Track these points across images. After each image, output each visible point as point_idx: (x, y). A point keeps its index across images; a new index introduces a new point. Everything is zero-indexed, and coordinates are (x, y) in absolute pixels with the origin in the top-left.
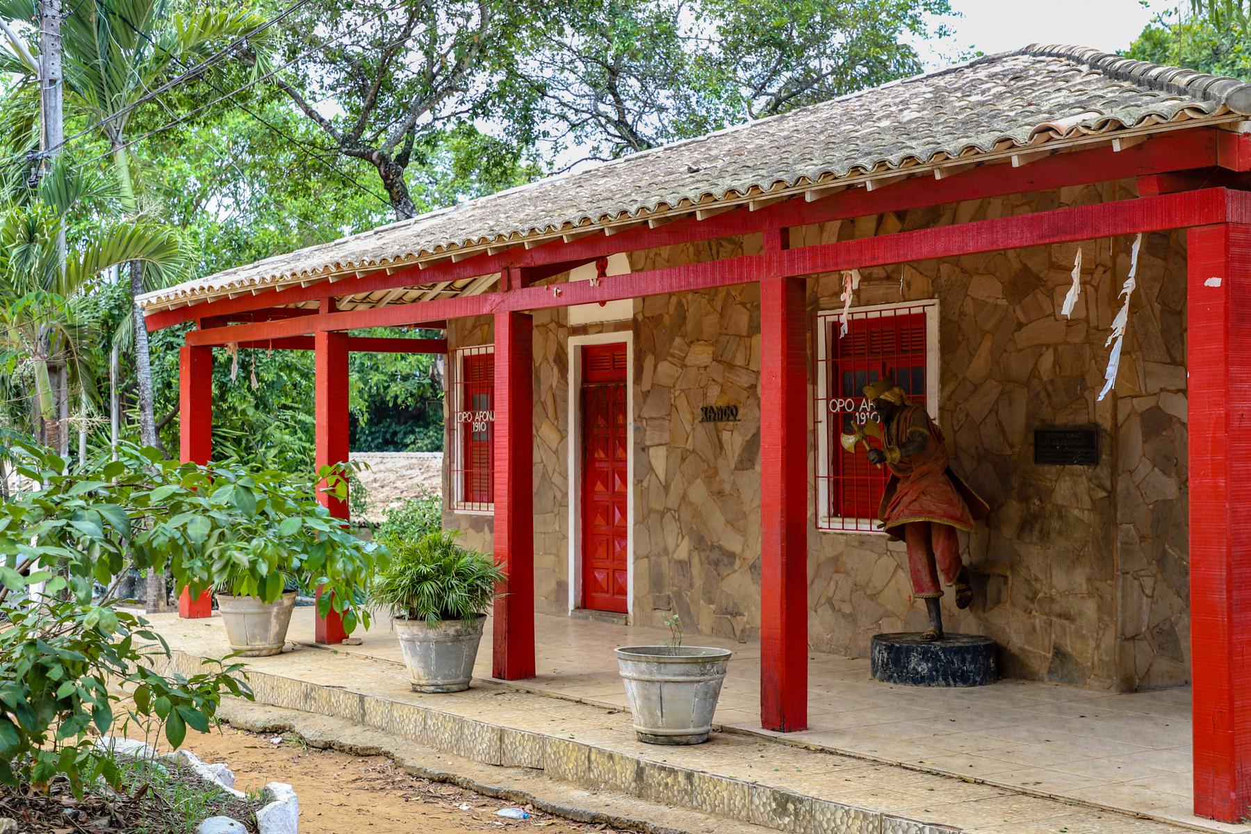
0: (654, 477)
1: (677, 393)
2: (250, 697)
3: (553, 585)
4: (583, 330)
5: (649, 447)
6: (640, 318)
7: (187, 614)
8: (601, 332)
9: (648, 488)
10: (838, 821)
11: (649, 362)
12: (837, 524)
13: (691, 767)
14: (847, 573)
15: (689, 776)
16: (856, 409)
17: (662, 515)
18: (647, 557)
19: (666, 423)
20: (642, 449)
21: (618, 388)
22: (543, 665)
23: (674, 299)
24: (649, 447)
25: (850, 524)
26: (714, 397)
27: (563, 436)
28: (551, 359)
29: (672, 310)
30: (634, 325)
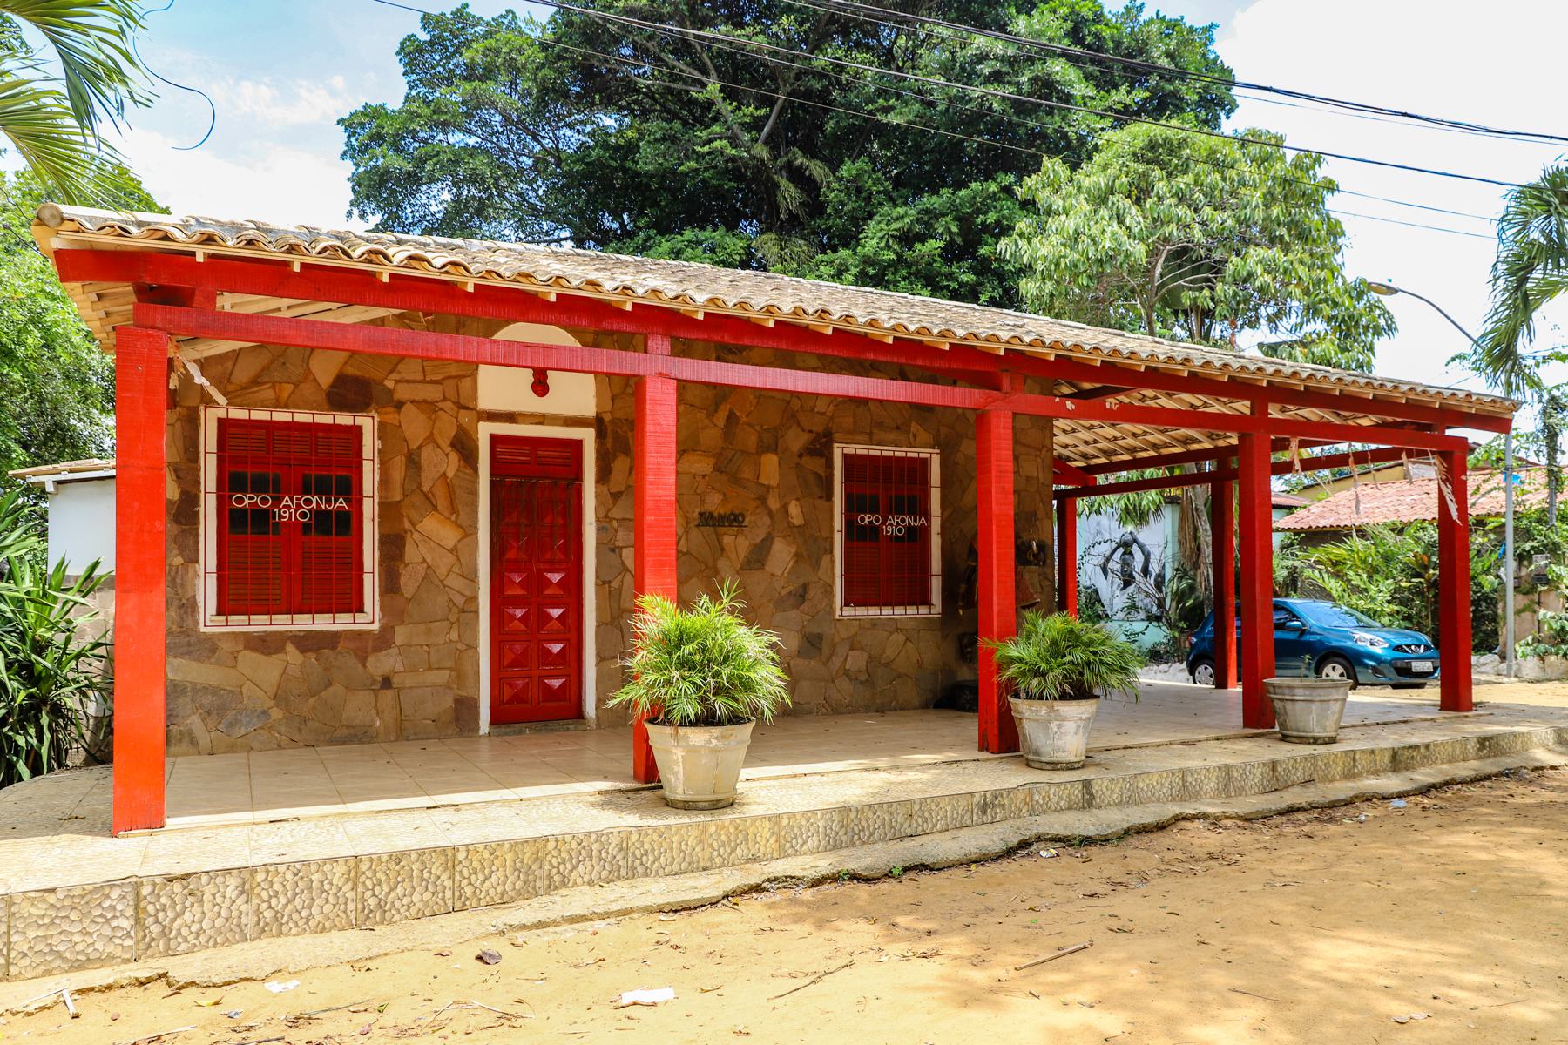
3: (449, 702)
4: (493, 416)
6: (607, 418)
7: (994, 741)
9: (620, 589)
10: (114, 923)
12: (849, 612)
13: (1427, 741)
14: (862, 649)
15: (1427, 746)
16: (884, 523)
22: (1478, 694)
25: (861, 611)
26: (714, 503)
27: (470, 531)
28: (445, 444)
30: (598, 423)
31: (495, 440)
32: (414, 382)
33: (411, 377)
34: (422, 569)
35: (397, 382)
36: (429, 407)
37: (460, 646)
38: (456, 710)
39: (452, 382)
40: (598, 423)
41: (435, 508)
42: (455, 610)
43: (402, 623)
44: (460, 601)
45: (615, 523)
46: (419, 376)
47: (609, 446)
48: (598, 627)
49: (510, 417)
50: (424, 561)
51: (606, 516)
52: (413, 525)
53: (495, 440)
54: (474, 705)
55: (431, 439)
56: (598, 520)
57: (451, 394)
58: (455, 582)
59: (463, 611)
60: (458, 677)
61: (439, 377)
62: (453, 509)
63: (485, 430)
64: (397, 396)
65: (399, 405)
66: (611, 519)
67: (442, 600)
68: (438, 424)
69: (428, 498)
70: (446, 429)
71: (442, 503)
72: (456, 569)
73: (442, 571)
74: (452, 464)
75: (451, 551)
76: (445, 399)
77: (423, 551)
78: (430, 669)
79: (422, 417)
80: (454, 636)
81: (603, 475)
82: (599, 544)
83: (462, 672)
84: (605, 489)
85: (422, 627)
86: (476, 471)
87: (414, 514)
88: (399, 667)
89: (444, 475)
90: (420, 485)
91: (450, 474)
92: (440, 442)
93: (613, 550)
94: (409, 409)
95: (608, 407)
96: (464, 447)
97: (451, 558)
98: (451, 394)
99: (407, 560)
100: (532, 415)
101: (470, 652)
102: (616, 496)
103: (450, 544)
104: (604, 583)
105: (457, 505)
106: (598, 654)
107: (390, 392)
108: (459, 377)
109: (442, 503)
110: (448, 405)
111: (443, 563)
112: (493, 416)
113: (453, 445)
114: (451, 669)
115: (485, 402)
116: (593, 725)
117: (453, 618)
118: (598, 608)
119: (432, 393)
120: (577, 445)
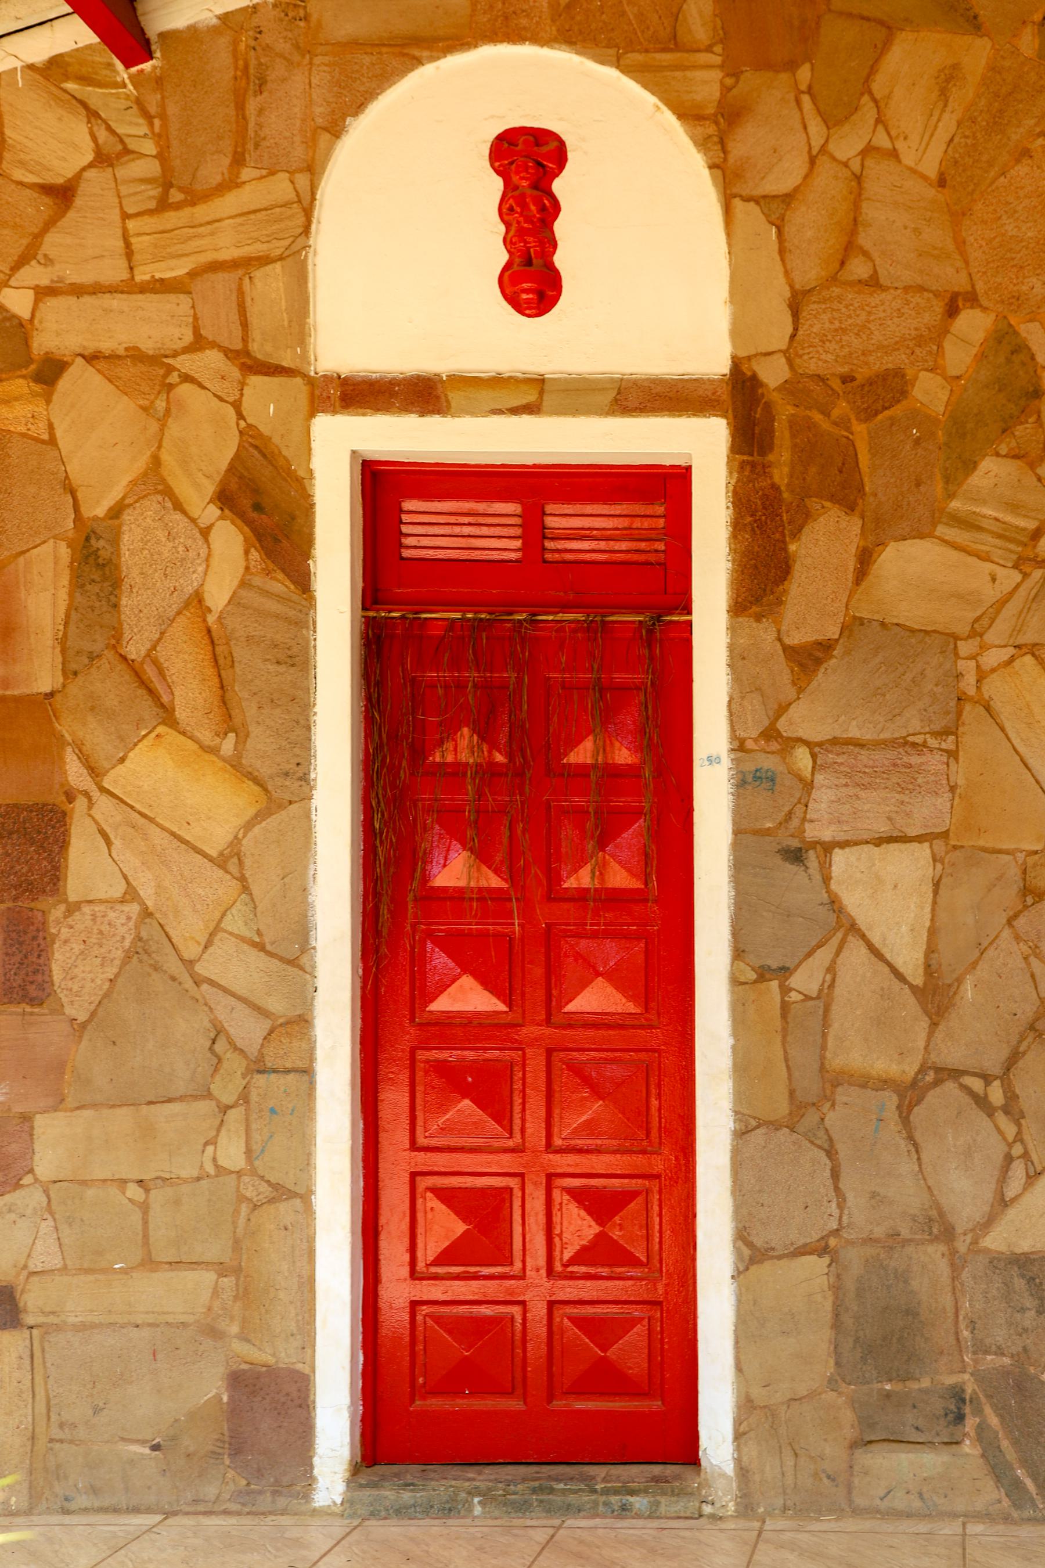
0: (856, 954)
1: (992, 658)
2: (486, 119)
3: (209, 1386)
4: (361, 394)
5: (828, 848)
6: (773, 374)
8: (531, 409)
9: (825, 996)
11: (823, 543)
17: (910, 1094)
18: (821, 1249)
19: (935, 762)
20: (777, 847)
21: (649, 635)
23: (973, 325)
24: (828, 848)
27: (284, 789)
29: (958, 357)
30: (741, 399)
31: (383, 486)
32: (96, 289)
33: (86, 276)
34: (122, 921)
35: (43, 293)
36: (149, 374)
37: (251, 1189)
38: (234, 1412)
39: (222, 283)
40: (741, 399)
41: (167, 715)
42: (234, 1064)
43: (58, 1103)
44: (248, 1030)
45: (802, 759)
46: (114, 271)
47: (780, 475)
48: (741, 1134)
49: (422, 394)
50: (131, 894)
51: (770, 733)
52: (95, 772)
53: (383, 486)
54: (295, 1396)
55: (154, 482)
56: (739, 747)
57: (222, 326)
58: (233, 967)
59: (259, 1067)
60: (244, 1295)
61: (178, 269)
62: (227, 715)
63: (336, 449)
64: (47, 340)
65: (49, 372)
66: (790, 743)
67: (189, 1028)
68: (174, 429)
69: (145, 681)
70: (203, 445)
71: (190, 692)
72: (235, 922)
73: (188, 929)
74: (226, 557)
75: (220, 862)
76: (199, 343)
77: (130, 861)
78: (149, 1263)
79: (124, 407)
80: (231, 1152)
81: (761, 580)
82: (744, 832)
83: (258, 1281)
84: (765, 633)
85: (122, 1119)
86: (302, 582)
87: (97, 737)
88: (46, 1255)
89: (197, 600)
90: (117, 635)
91: (218, 596)
92: (184, 489)
93: (795, 856)
94: (79, 383)
95: (776, 332)
96: (266, 508)
97: (218, 886)
98: (222, 326)
99: (74, 887)
100: (498, 382)
101: (286, 1210)
102: (808, 659)
103: (217, 836)
104: (763, 974)
105: (246, 704)
106: (742, 1236)
107: (20, 330)
108: (246, 264)
109: (190, 692)
110: (209, 363)
111: (189, 905)
112: (361, 394)
113: (224, 498)
114: (222, 1269)
115: (345, 341)
116: (724, 1496)
117: (226, 1090)
118: (743, 1069)
119: (153, 325)
120: (670, 485)
